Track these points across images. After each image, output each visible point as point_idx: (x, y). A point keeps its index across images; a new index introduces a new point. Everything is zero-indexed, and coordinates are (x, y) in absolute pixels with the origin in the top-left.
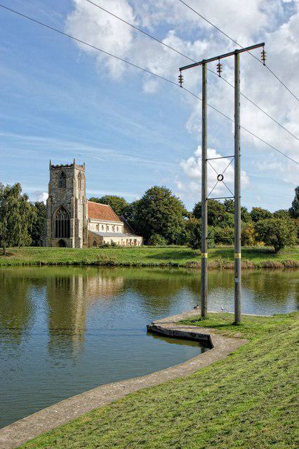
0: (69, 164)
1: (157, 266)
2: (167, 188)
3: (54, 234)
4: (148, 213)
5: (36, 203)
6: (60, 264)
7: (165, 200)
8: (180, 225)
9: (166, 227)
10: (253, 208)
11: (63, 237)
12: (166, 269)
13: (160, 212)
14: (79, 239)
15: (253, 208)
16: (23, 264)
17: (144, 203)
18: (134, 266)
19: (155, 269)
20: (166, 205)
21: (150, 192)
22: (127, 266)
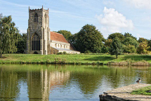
0: (40, 9)
1: (90, 64)
2: (94, 25)
3: (31, 49)
4: (84, 39)
5: (23, 34)
6: (33, 63)
7: (93, 32)
8: (101, 46)
9: (92, 46)
10: (140, 38)
11: (36, 50)
12: (96, 66)
13: (90, 38)
14: (45, 51)
15: (140, 38)
16: (12, 63)
17: (81, 33)
18: (77, 64)
19: (89, 66)
20: (93, 35)
21: (84, 28)
22: (73, 64)
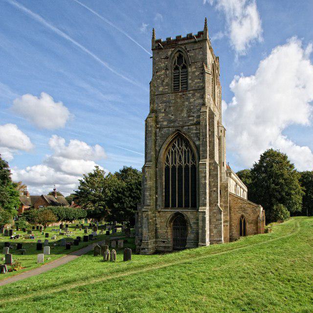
0: (195, 33)
11: (180, 206)
